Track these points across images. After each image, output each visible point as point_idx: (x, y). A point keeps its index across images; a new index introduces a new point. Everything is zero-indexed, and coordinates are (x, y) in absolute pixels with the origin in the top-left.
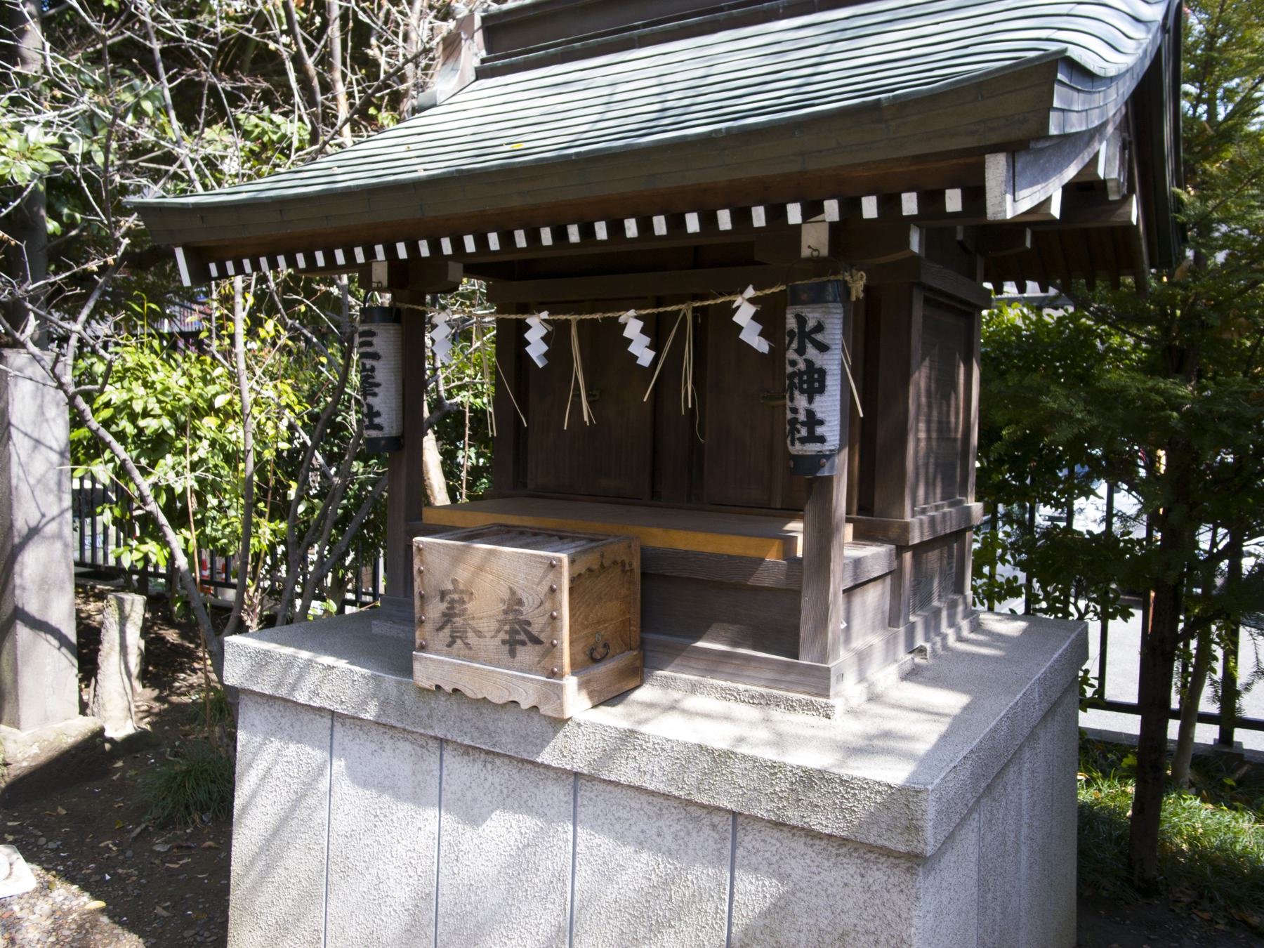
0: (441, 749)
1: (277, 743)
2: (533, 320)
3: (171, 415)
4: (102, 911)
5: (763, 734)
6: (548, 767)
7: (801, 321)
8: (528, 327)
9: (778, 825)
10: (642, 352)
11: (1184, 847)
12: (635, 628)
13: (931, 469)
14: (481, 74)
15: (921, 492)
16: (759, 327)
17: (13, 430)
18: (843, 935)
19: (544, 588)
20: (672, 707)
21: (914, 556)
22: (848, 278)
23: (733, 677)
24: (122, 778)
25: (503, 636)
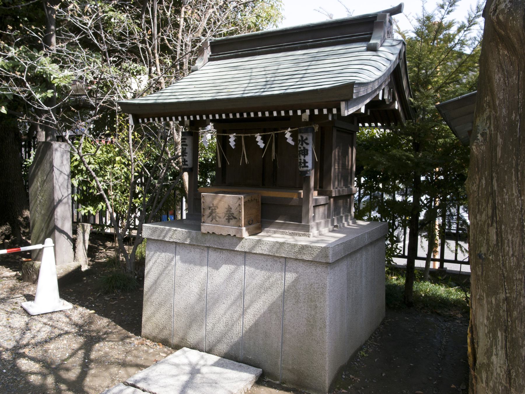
0: (208, 250)
1: (158, 253)
2: (231, 136)
3: (99, 164)
4: (95, 313)
5: (292, 240)
7: (302, 137)
8: (230, 138)
9: (296, 259)
10: (261, 145)
11: (423, 295)
12: (260, 217)
13: (340, 177)
14: (210, 60)
15: (336, 183)
16: (292, 138)
17: (54, 168)
18: (312, 284)
19: (237, 204)
20: (269, 236)
21: (334, 200)
22: (314, 126)
23: (285, 229)
24: (87, 282)
25: (226, 217)
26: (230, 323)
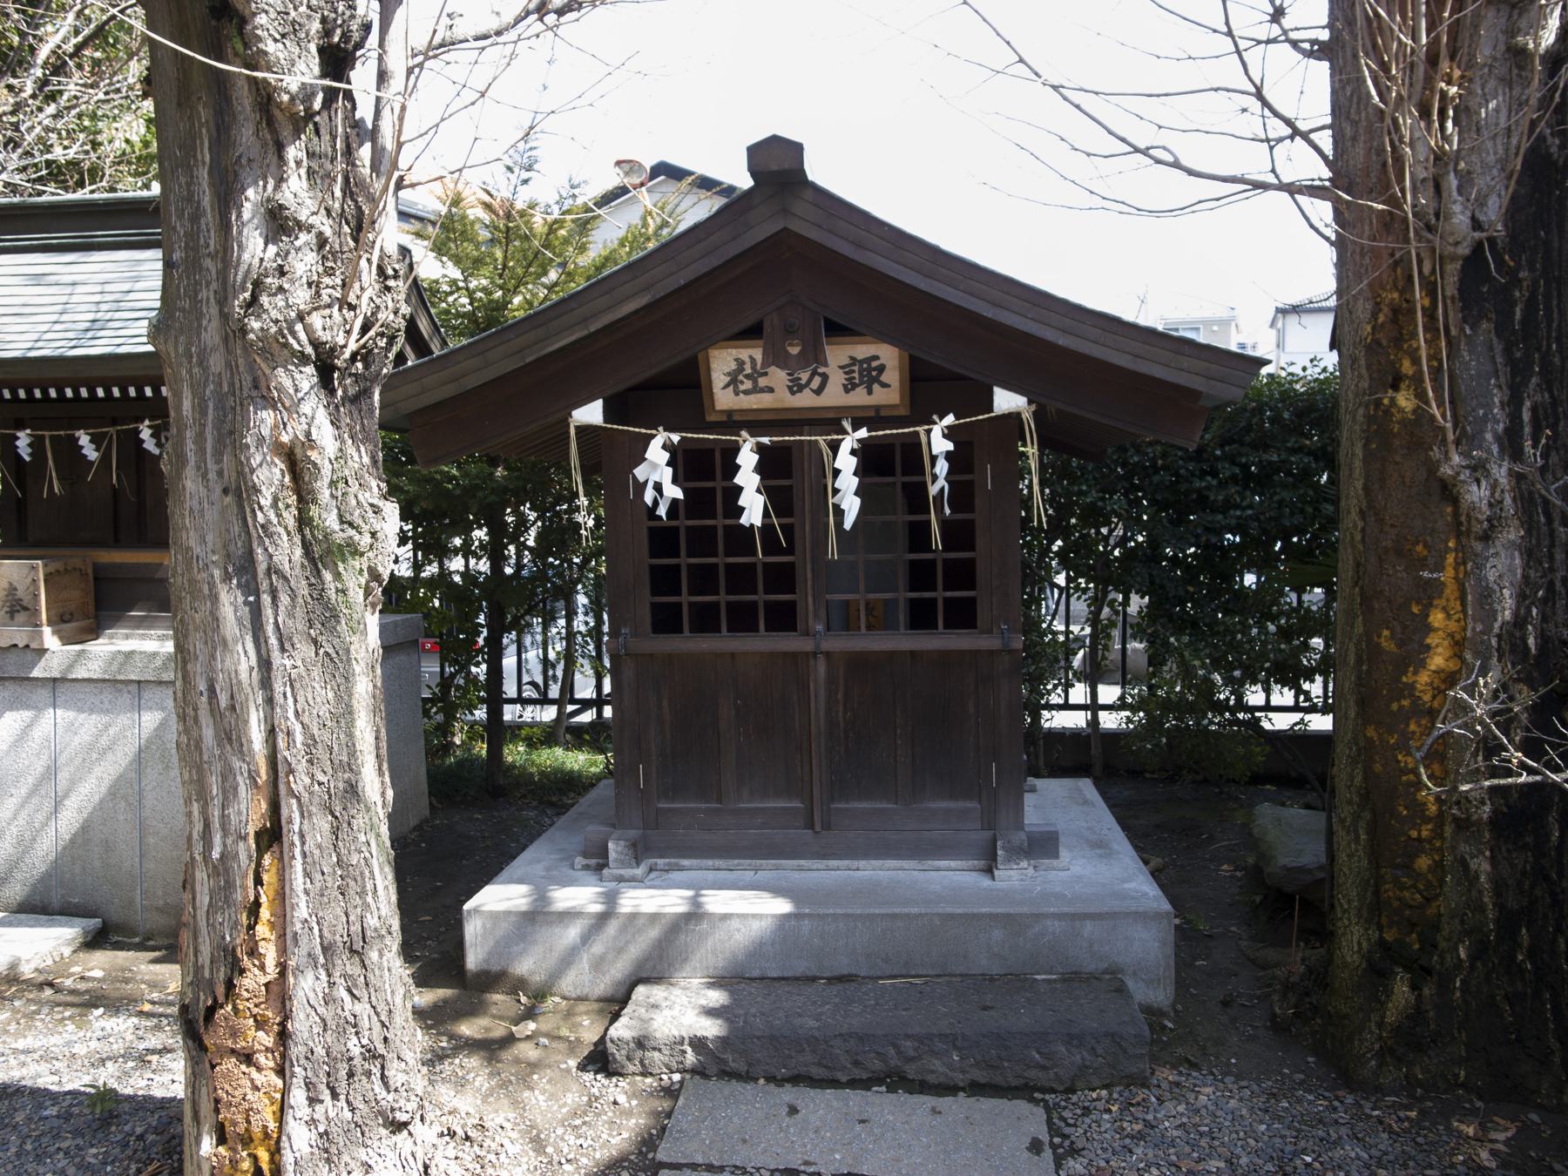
6: (37, 679)
10: (91, 453)
12: (91, 608)
23: (149, 628)
26: (27, 835)
